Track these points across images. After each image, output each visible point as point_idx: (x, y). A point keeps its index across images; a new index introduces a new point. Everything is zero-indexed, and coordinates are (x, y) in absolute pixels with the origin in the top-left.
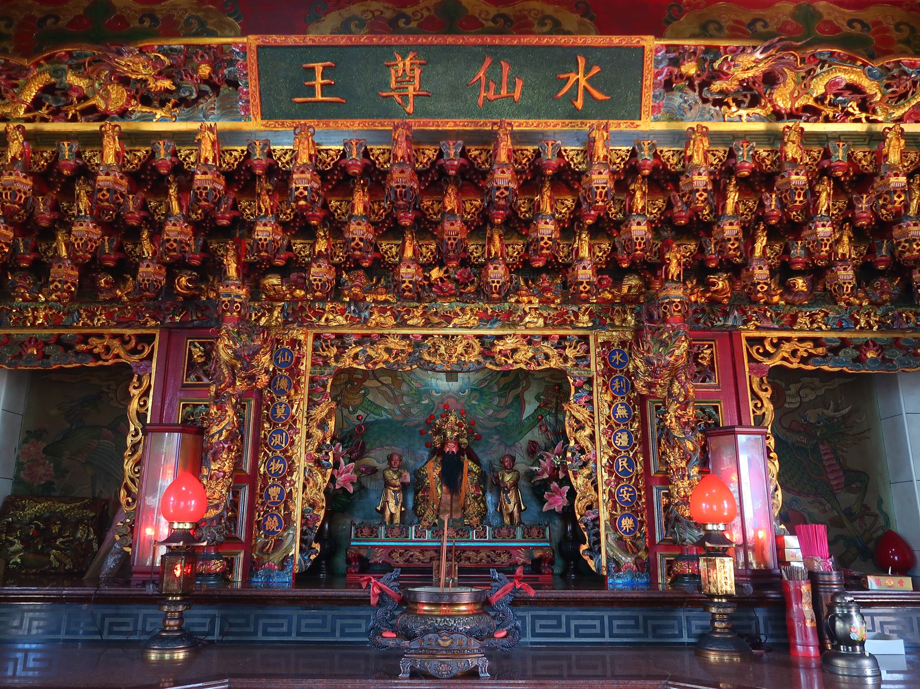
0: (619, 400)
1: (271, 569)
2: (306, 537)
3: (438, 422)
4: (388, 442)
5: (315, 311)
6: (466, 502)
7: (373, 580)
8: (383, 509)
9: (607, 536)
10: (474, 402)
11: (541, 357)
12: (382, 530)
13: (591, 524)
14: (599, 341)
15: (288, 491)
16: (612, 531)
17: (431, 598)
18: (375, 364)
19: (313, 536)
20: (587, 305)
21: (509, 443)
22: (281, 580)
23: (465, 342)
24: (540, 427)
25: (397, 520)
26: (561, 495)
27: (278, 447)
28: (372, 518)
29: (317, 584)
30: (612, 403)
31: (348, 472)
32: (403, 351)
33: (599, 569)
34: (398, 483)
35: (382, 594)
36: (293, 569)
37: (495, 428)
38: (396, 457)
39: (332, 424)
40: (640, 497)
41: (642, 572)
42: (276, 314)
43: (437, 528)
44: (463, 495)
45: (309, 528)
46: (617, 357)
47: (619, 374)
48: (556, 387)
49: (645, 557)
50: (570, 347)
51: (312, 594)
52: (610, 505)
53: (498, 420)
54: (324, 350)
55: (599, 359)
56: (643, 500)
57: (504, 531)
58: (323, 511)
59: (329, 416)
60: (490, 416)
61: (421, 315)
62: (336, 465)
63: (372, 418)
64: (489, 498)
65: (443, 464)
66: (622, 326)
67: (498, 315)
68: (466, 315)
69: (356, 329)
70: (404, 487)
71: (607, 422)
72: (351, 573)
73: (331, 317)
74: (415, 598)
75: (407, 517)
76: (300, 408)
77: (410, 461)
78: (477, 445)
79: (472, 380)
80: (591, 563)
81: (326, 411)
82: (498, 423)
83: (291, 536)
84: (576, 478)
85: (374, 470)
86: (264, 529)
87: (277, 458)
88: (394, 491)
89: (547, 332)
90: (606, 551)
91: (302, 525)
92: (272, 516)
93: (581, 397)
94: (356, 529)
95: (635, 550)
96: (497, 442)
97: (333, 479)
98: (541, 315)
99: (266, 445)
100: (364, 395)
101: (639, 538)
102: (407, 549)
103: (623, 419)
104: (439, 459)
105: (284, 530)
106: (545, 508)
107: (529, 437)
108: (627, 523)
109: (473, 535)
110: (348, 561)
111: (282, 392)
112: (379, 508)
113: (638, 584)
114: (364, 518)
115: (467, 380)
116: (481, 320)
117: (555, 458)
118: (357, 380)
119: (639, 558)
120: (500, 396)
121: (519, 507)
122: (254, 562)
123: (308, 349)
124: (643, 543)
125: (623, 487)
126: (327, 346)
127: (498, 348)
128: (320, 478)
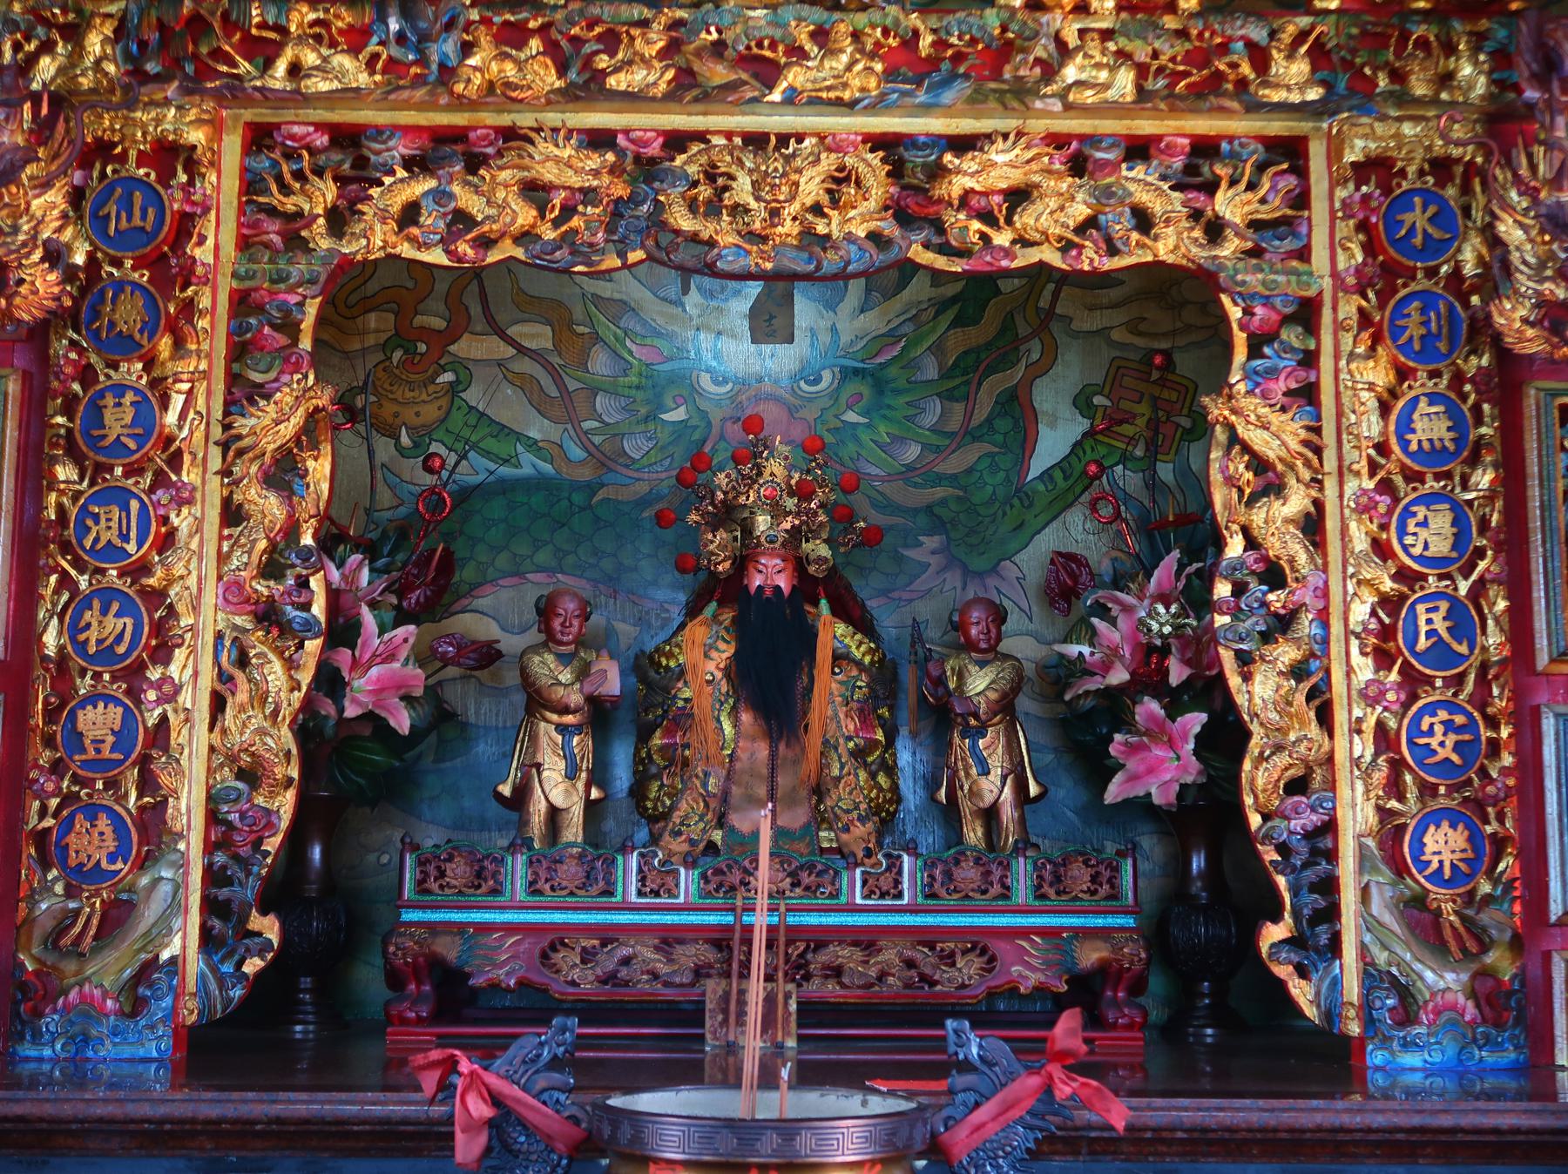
0: (1421, 383)
1: (90, 1010)
2: (224, 893)
4: (543, 557)
5: (247, 36)
6: (822, 767)
7: (465, 1066)
8: (522, 793)
9: (1365, 893)
10: (851, 417)
11: (1120, 225)
12: (518, 869)
13: (1303, 848)
14: (1350, 157)
15: (152, 719)
16: (1385, 875)
17: (707, 1140)
18: (485, 243)
19: (249, 891)
20: (1304, 21)
21: (978, 563)
22: (127, 1052)
23: (828, 162)
24: (1093, 507)
26: (1172, 744)
27: (112, 552)
28: (484, 825)
29: (277, 1070)
30: (1393, 393)
31: (390, 657)
32: (589, 195)
33: (1331, 1014)
34: (575, 699)
35: (504, 1117)
36: (175, 1010)
37: (929, 509)
38: (569, 605)
39: (319, 468)
40: (1495, 747)
41: (1499, 1025)
42: (94, 43)
43: (720, 862)
44: (814, 741)
45: (236, 857)
46: (1417, 217)
47: (1421, 283)
48: (1164, 341)
49: (1507, 971)
50: (1233, 183)
51: (230, 1111)
52: (1380, 775)
53: (939, 479)
54: (285, 190)
55: (1345, 228)
56: (1507, 760)
57: (968, 873)
58: (290, 796)
59: (308, 436)
60: (910, 468)
61: (663, 54)
62: (341, 630)
63: (475, 470)
64: (905, 756)
65: (742, 631)
66: (1435, 101)
67: (959, 57)
68: (834, 53)
69: (407, 105)
70: (600, 716)
71: (1373, 468)
72: (404, 1021)
73: (310, 58)
74: (637, 1139)
75: (609, 824)
76: (190, 412)
78: (862, 571)
79: (845, 339)
80: (1302, 993)
81: (297, 420)
82: (940, 492)
83: (165, 889)
84: (1247, 677)
85: (488, 655)
86: (64, 865)
87: (107, 596)
88: (562, 729)
89: (1145, 126)
90: (1363, 950)
91: (209, 848)
92: (92, 812)
93: (1272, 373)
94: (421, 863)
95: (1472, 946)
97: (329, 681)
98: (1122, 55)
99: (66, 548)
100: (454, 389)
101: (1488, 899)
102: (609, 936)
103: (1434, 453)
104: (727, 616)
105: (142, 864)
106: (1115, 791)
107: (1048, 541)
108: (1443, 845)
109: (853, 885)
110: (395, 979)
111: (122, 346)
112: (506, 790)
113: (1483, 1071)
115: (825, 338)
116: (890, 74)
117: (1152, 614)
118: (426, 333)
119: (1484, 973)
120: (948, 396)
122: (23, 987)
123: (223, 183)
124: (1501, 920)
125: (1431, 709)
126: (299, 175)
127: (957, 185)
128: (275, 675)
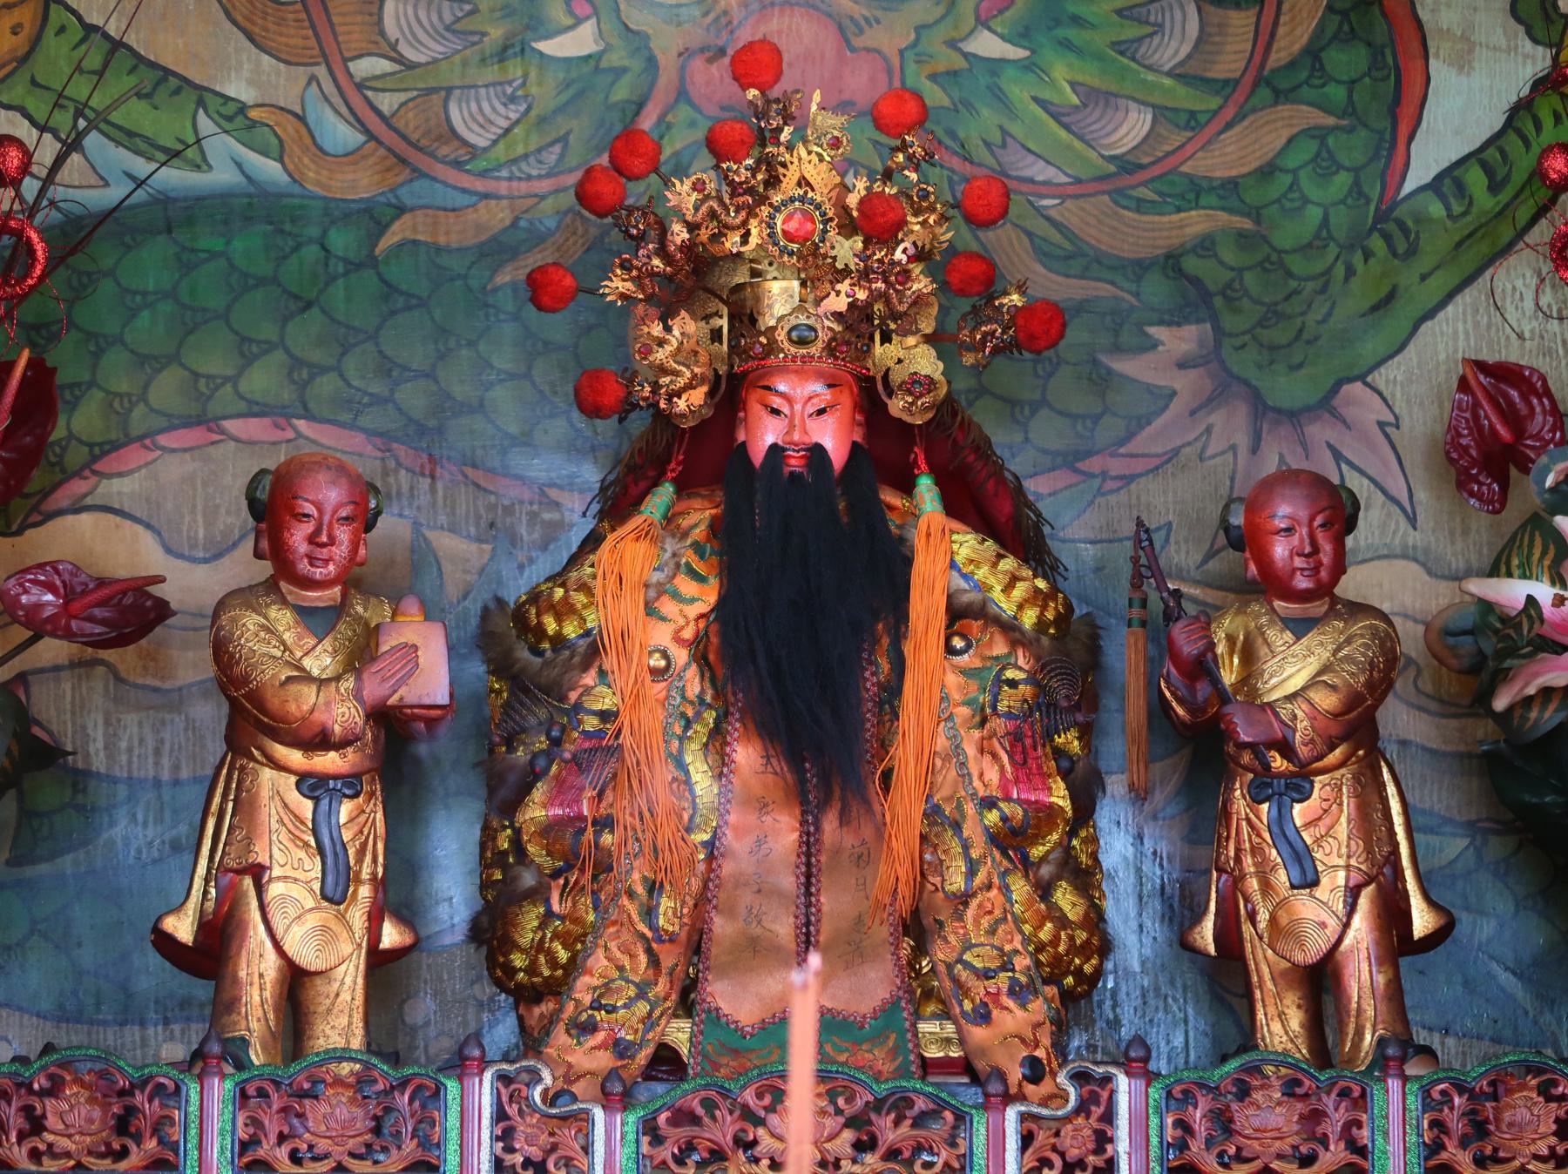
3: (683, 195)
4: (262, 380)
10: (987, 45)
21: (1287, 389)
25: (340, 1023)
28: (129, 1013)
34: (343, 714)
37: (1171, 263)
38: (327, 495)
44: (904, 809)
53: (1195, 192)
60: (1126, 165)
63: (101, 176)
64: (1123, 844)
65: (732, 547)
75: (422, 1008)
77: (447, 544)
82: (1197, 222)
85: (134, 613)
88: (312, 784)
96: (1186, 384)
104: (699, 517)
107: (1454, 336)
112: (182, 928)
114: (63, 1016)
121: (1393, 914)
